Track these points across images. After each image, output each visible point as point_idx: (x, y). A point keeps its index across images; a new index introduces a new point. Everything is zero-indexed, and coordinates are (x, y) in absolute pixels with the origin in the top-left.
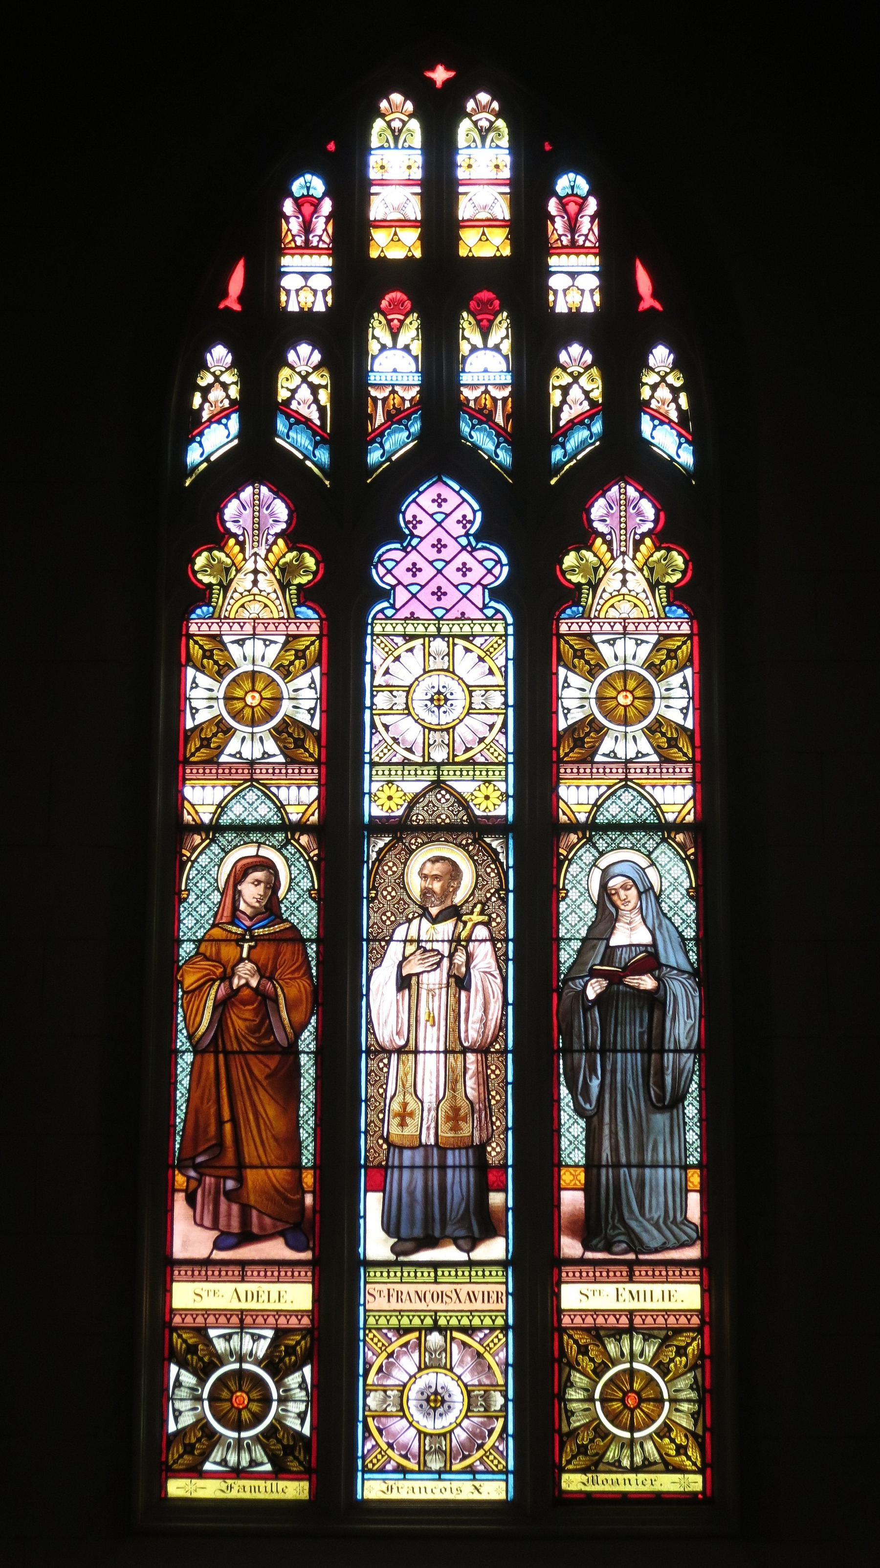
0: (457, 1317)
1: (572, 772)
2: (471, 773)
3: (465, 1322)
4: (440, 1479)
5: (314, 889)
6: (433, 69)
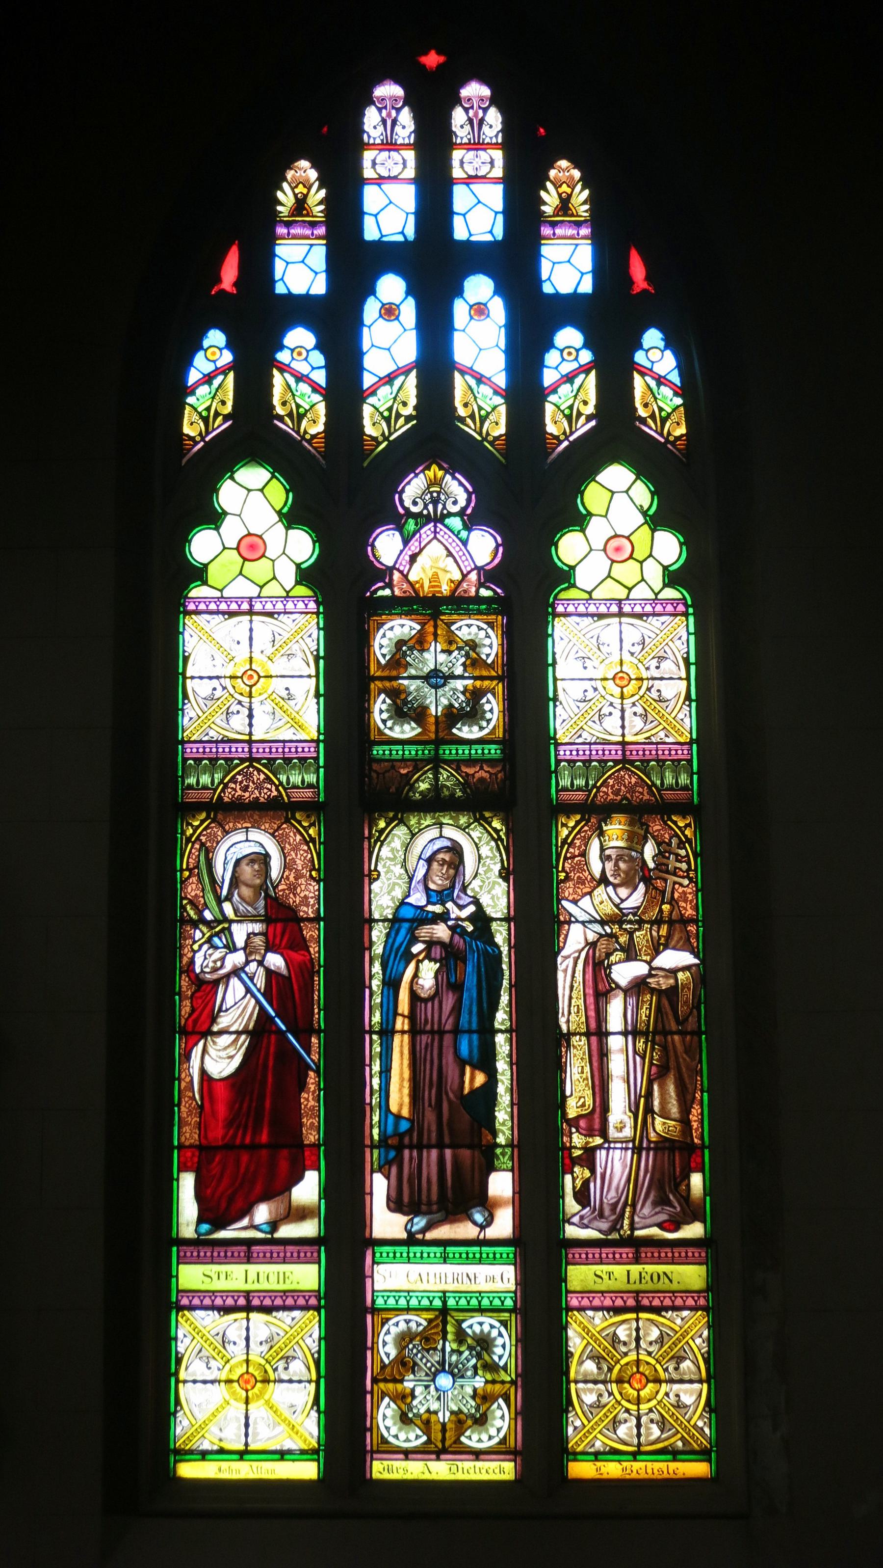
0: (466, 1298)
1: (610, 751)
2: (287, 750)
3: (267, 1302)
4: (635, 1460)
5: (314, 869)
6: (426, 53)
